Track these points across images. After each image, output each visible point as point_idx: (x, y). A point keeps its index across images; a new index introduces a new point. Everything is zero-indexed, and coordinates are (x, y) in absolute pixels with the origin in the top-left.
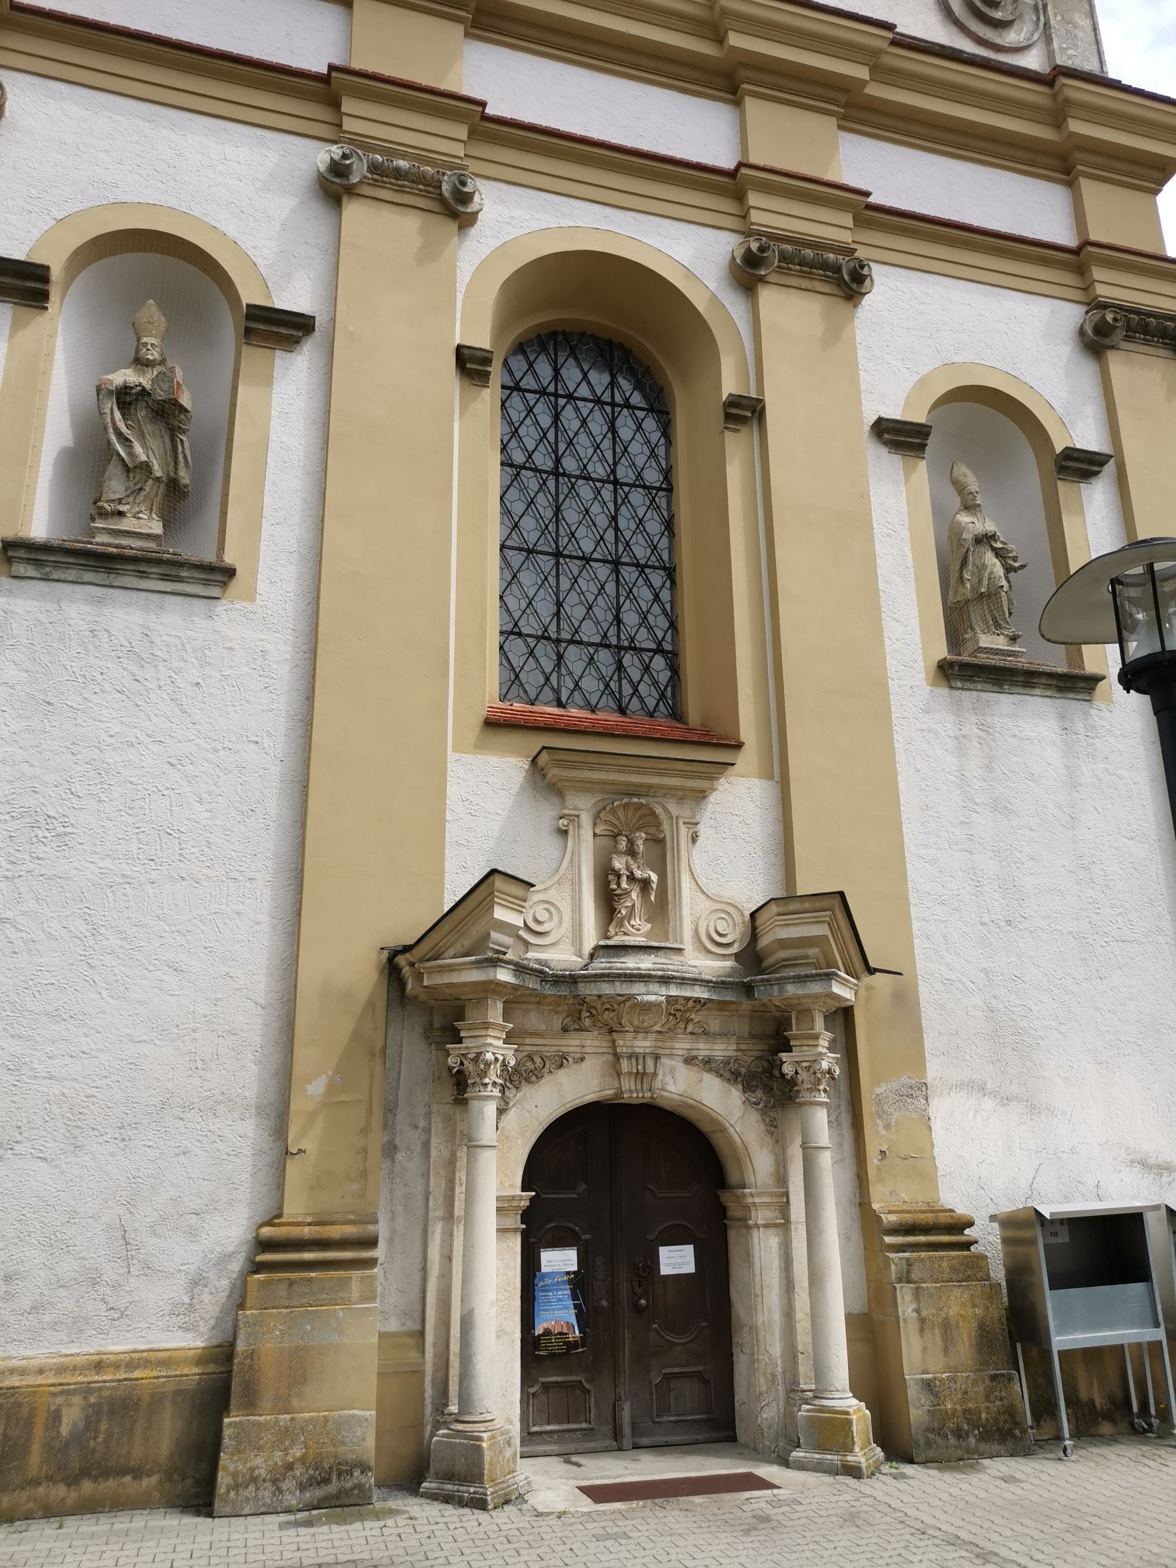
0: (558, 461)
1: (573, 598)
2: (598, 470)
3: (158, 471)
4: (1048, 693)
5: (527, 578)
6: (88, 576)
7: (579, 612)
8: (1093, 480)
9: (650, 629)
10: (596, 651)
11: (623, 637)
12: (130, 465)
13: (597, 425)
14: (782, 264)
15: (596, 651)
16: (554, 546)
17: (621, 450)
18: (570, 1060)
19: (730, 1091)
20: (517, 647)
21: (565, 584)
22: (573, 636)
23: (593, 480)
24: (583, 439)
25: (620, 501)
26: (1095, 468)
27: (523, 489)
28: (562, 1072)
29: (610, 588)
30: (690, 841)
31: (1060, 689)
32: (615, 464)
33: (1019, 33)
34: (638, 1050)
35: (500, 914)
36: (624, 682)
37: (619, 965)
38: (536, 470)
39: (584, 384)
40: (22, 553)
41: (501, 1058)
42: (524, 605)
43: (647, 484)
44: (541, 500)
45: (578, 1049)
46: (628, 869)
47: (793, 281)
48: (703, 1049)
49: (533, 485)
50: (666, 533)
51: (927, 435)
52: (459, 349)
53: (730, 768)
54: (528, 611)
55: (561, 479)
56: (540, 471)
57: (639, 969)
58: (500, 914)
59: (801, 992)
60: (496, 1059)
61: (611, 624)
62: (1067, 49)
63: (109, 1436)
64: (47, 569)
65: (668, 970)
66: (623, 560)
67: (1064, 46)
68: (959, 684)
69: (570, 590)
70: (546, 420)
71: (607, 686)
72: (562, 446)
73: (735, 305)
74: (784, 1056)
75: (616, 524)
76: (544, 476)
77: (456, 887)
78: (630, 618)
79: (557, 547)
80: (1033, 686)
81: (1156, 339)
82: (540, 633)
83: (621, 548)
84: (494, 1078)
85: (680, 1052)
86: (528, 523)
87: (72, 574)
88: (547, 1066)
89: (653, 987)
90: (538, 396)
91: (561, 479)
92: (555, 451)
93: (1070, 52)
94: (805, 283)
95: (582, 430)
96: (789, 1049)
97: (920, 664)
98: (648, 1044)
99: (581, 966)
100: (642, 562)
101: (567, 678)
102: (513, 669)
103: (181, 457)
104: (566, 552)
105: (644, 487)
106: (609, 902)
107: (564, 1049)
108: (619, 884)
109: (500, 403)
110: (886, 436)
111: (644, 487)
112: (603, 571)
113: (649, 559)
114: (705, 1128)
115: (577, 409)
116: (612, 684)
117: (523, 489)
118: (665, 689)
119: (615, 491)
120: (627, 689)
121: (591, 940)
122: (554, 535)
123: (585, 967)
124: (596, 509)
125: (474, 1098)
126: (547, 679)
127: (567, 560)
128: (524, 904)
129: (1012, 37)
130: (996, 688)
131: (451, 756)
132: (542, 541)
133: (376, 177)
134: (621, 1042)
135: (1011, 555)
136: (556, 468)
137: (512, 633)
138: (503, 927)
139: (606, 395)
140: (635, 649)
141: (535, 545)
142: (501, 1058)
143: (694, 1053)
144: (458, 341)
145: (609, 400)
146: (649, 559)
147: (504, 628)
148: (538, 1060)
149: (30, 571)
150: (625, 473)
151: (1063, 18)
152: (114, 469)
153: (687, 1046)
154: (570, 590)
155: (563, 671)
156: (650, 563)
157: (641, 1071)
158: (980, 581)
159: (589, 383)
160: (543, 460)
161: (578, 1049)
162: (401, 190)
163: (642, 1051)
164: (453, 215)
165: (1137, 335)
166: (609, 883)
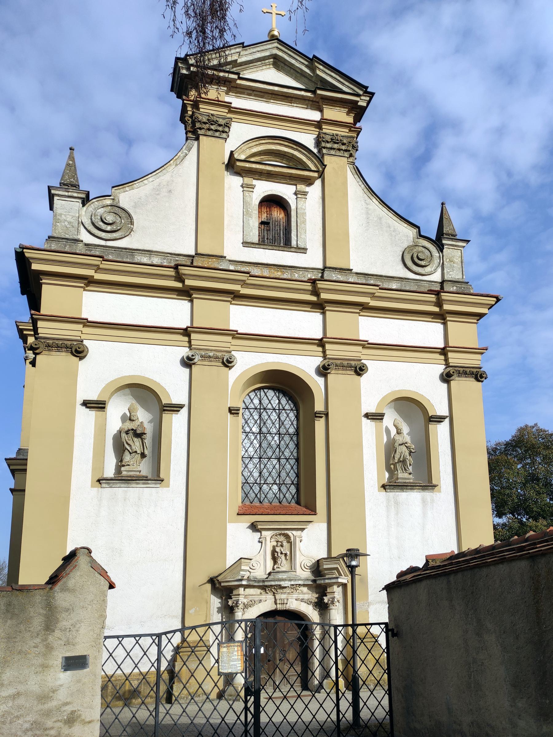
0: (260, 430)
1: (265, 470)
2: (274, 430)
3: (139, 452)
4: (419, 491)
5: (251, 466)
6: (122, 485)
7: (267, 474)
8: (442, 423)
9: (290, 477)
10: (272, 486)
11: (281, 481)
12: (131, 452)
13: (274, 416)
14: (336, 368)
15: (272, 486)
16: (259, 456)
17: (282, 423)
18: (262, 601)
19: (309, 606)
20: (247, 488)
21: (262, 466)
22: (269, 432)
23: (272, 434)
24: (269, 421)
25: (281, 439)
26: (442, 420)
27: (249, 439)
28: (260, 604)
29: (277, 466)
30: (300, 541)
31: (423, 489)
32: (279, 428)
33: (432, 268)
34: (282, 598)
35: (243, 568)
36: (281, 494)
37: (277, 577)
38: (253, 433)
39: (270, 404)
40: (104, 481)
41: (243, 602)
42: (249, 474)
43: (290, 433)
44: (255, 441)
45: (265, 598)
46: (280, 550)
47: (340, 372)
48: (301, 596)
49: (253, 437)
50: (296, 448)
51: (383, 416)
52: (229, 408)
53: (311, 524)
54: (250, 476)
55: (261, 435)
56: (254, 433)
57: (282, 578)
58: (243, 568)
59: (330, 582)
60: (242, 603)
61: (277, 477)
62: (450, 272)
63: (144, 689)
64: (111, 485)
65: (291, 578)
66: (281, 458)
67: (449, 271)
68: (389, 491)
69: (264, 468)
70: (256, 417)
71: (276, 496)
72: (262, 424)
73: (321, 381)
74: (325, 598)
75: (279, 447)
76: (256, 434)
77: (229, 563)
78: (283, 474)
79: (260, 456)
80: (414, 489)
81: (469, 376)
82: (254, 482)
83: (281, 454)
84: (241, 607)
85: (295, 597)
86: (251, 449)
87: (118, 485)
88: (256, 603)
89: (287, 582)
90: (254, 410)
91: (261, 435)
92: (260, 427)
93: (451, 273)
94: (344, 372)
95: (269, 419)
96: (326, 596)
97: (377, 485)
98: (285, 596)
99: (265, 578)
100: (288, 458)
101: (263, 495)
102: (245, 493)
103: (145, 446)
104: (263, 457)
105: (289, 434)
106: (275, 559)
107: (261, 598)
108: (277, 555)
109: (242, 427)
110: (370, 417)
111: (289, 434)
112: (275, 461)
113: (290, 457)
114: (302, 616)
115: (267, 412)
116: (277, 495)
117: (249, 439)
118: (294, 495)
119: (279, 437)
120: (282, 496)
121: (269, 569)
122: (259, 469)
123: (267, 578)
124: (273, 443)
125: (236, 612)
126: (256, 495)
127: (263, 459)
128: (250, 564)
129: (428, 269)
130: (401, 491)
131: (228, 524)
132: (255, 455)
133: (202, 359)
134: (277, 596)
135: (412, 448)
136: (260, 432)
137: (245, 483)
138: (243, 570)
139: (277, 407)
140: (285, 484)
141: (253, 456)
142: (243, 602)
143: (299, 597)
144: (229, 406)
145: (278, 408)
146: (290, 457)
147: (243, 482)
148: (253, 602)
149: (106, 486)
150: (283, 431)
151: (450, 260)
152: (127, 453)
153: (297, 596)
154: (264, 468)
155: (262, 493)
156: (290, 458)
157: (283, 603)
158: (400, 457)
159: (271, 404)
160: (255, 429)
161: (265, 598)
162: (211, 361)
163: (283, 598)
164: (227, 366)
165: (462, 375)
166: (275, 555)
